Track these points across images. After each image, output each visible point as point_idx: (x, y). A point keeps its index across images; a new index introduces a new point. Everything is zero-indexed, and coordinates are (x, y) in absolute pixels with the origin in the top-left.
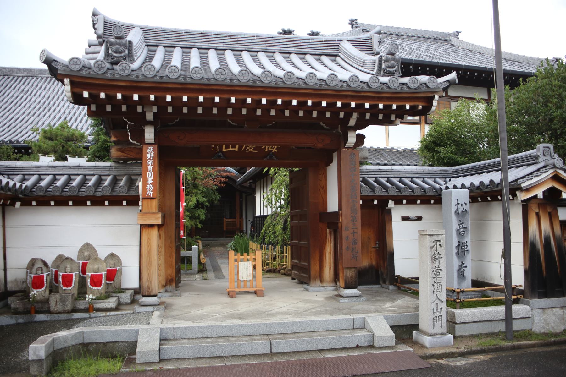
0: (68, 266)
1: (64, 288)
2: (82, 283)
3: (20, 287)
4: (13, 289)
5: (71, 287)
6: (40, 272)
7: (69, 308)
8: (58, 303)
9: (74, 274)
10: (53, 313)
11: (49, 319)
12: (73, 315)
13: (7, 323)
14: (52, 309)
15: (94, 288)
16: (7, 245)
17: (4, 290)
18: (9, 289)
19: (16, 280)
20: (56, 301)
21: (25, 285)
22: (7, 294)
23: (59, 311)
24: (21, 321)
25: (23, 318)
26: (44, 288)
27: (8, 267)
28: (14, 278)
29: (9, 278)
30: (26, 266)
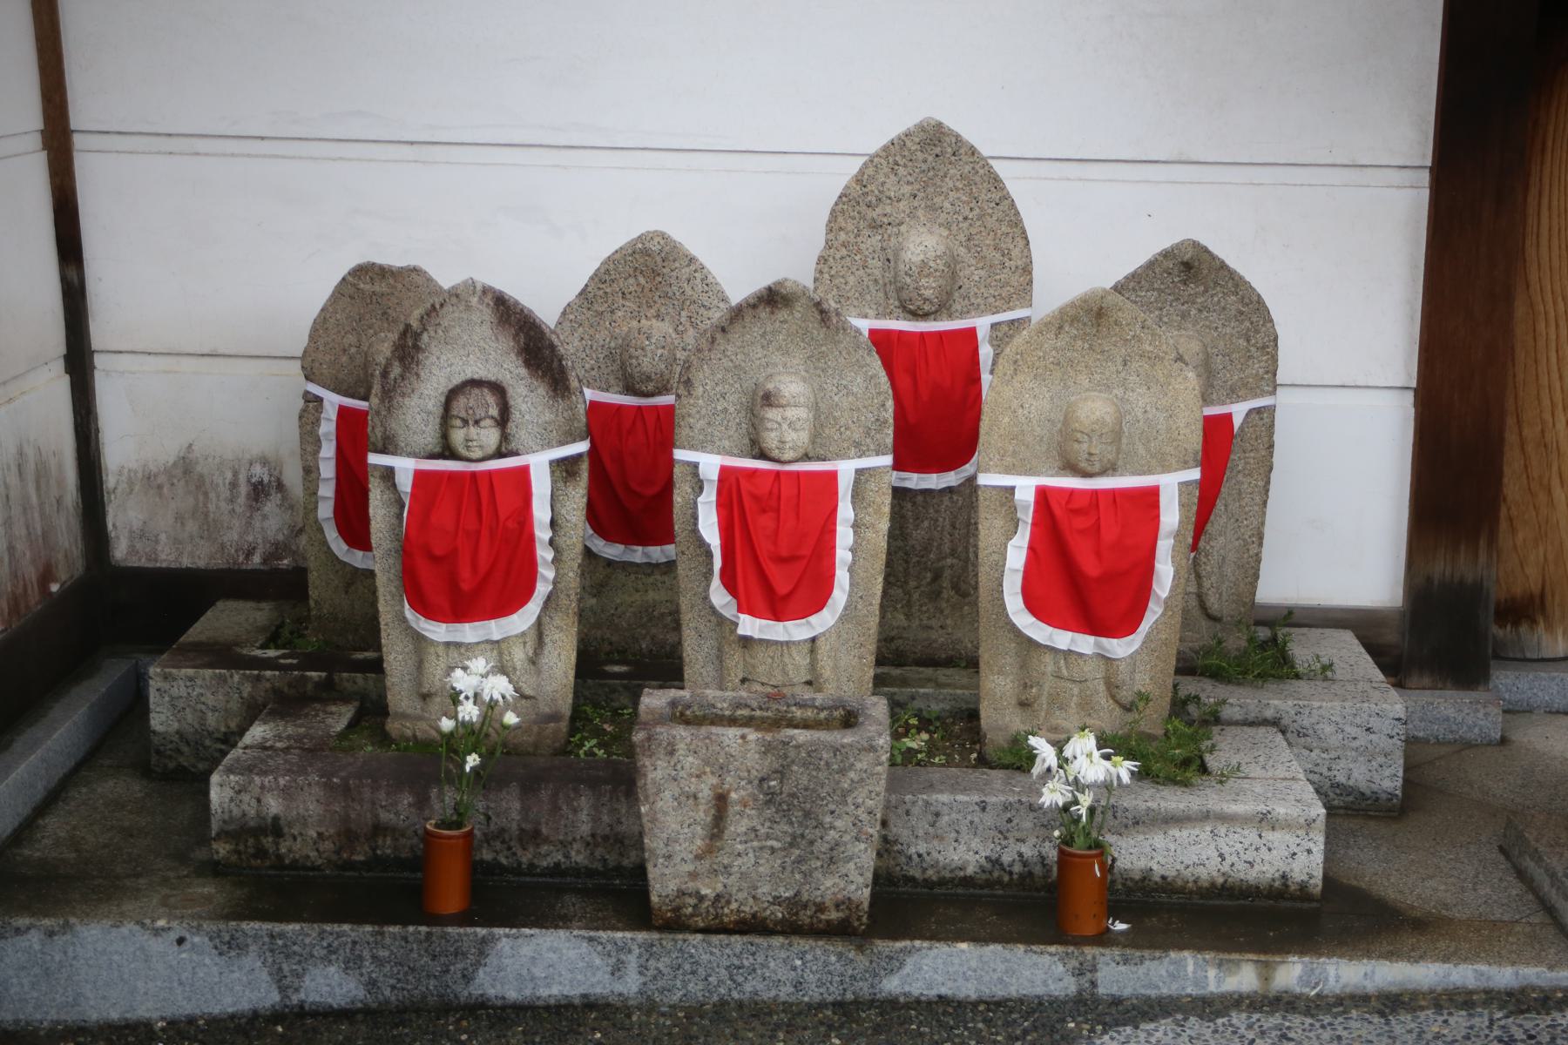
0: (792, 387)
1: (749, 626)
2: (930, 561)
3: (232, 536)
4: (167, 557)
5: (823, 621)
6: (489, 436)
7: (851, 880)
8: (738, 826)
9: (845, 469)
10: (675, 924)
11: (631, 984)
12: (893, 964)
13: (184, 1006)
14: (664, 882)
15: (1063, 639)
16: (81, 114)
17: (79, 567)
18: (121, 551)
19: (185, 470)
20: (721, 800)
21: (272, 522)
22: (116, 610)
23: (742, 904)
24: (330, 985)
25: (352, 963)
26: (522, 620)
27: (101, 333)
28: (165, 451)
29: (120, 451)
30: (297, 339)
